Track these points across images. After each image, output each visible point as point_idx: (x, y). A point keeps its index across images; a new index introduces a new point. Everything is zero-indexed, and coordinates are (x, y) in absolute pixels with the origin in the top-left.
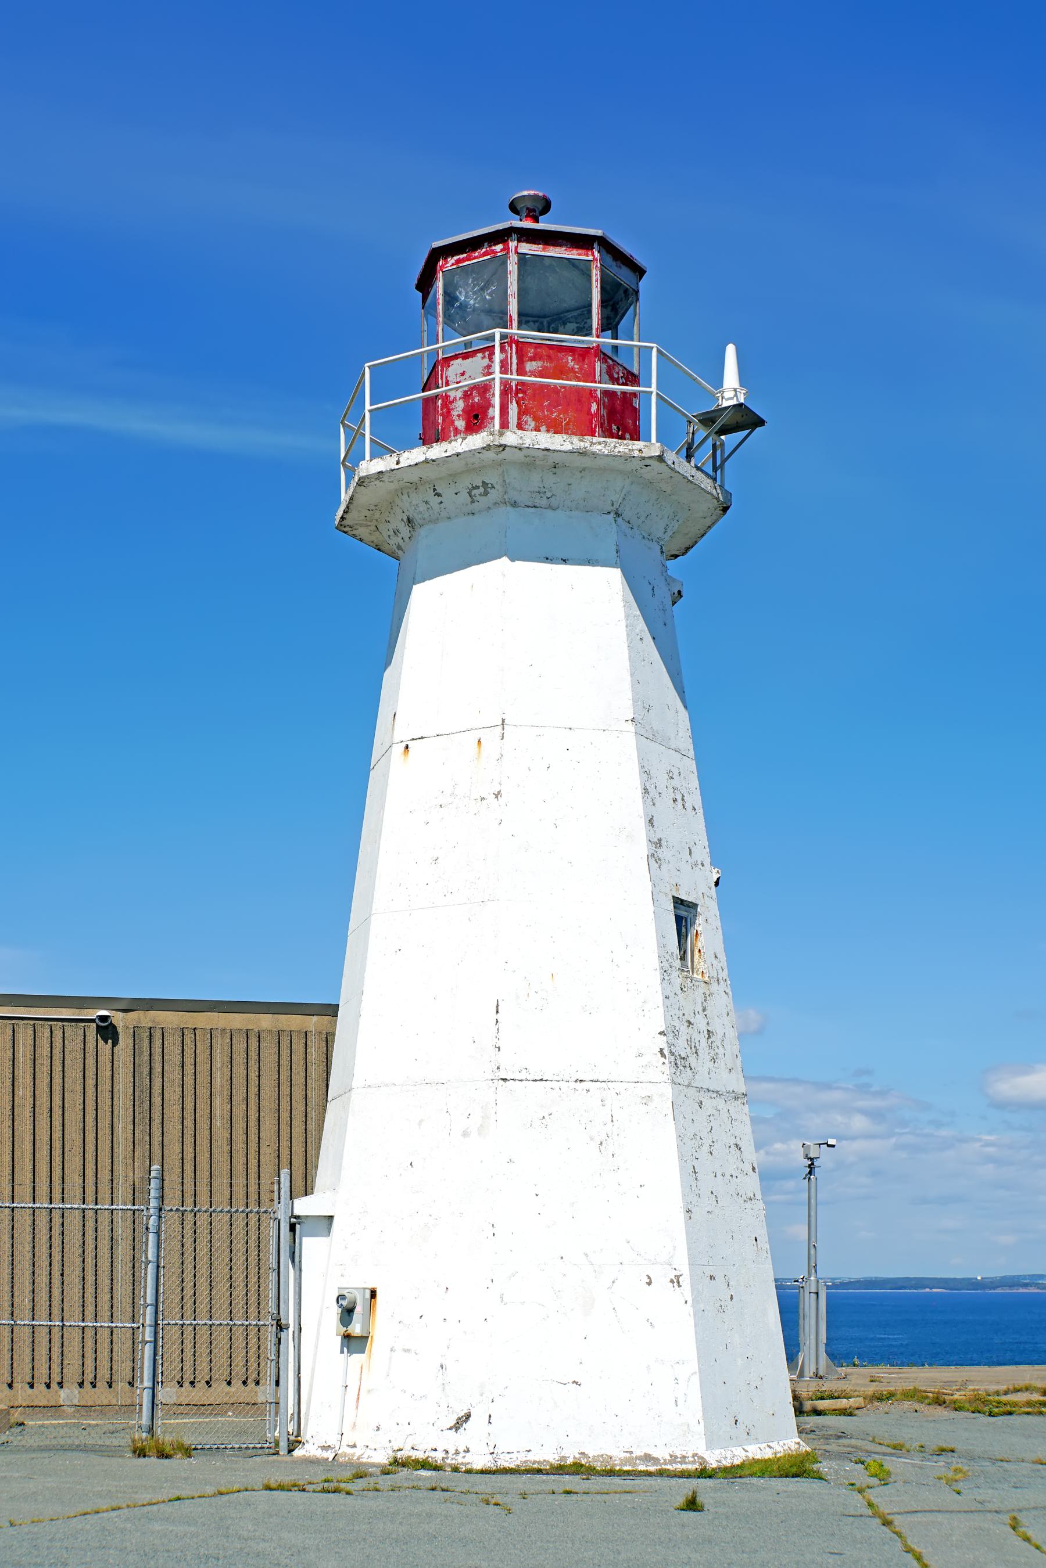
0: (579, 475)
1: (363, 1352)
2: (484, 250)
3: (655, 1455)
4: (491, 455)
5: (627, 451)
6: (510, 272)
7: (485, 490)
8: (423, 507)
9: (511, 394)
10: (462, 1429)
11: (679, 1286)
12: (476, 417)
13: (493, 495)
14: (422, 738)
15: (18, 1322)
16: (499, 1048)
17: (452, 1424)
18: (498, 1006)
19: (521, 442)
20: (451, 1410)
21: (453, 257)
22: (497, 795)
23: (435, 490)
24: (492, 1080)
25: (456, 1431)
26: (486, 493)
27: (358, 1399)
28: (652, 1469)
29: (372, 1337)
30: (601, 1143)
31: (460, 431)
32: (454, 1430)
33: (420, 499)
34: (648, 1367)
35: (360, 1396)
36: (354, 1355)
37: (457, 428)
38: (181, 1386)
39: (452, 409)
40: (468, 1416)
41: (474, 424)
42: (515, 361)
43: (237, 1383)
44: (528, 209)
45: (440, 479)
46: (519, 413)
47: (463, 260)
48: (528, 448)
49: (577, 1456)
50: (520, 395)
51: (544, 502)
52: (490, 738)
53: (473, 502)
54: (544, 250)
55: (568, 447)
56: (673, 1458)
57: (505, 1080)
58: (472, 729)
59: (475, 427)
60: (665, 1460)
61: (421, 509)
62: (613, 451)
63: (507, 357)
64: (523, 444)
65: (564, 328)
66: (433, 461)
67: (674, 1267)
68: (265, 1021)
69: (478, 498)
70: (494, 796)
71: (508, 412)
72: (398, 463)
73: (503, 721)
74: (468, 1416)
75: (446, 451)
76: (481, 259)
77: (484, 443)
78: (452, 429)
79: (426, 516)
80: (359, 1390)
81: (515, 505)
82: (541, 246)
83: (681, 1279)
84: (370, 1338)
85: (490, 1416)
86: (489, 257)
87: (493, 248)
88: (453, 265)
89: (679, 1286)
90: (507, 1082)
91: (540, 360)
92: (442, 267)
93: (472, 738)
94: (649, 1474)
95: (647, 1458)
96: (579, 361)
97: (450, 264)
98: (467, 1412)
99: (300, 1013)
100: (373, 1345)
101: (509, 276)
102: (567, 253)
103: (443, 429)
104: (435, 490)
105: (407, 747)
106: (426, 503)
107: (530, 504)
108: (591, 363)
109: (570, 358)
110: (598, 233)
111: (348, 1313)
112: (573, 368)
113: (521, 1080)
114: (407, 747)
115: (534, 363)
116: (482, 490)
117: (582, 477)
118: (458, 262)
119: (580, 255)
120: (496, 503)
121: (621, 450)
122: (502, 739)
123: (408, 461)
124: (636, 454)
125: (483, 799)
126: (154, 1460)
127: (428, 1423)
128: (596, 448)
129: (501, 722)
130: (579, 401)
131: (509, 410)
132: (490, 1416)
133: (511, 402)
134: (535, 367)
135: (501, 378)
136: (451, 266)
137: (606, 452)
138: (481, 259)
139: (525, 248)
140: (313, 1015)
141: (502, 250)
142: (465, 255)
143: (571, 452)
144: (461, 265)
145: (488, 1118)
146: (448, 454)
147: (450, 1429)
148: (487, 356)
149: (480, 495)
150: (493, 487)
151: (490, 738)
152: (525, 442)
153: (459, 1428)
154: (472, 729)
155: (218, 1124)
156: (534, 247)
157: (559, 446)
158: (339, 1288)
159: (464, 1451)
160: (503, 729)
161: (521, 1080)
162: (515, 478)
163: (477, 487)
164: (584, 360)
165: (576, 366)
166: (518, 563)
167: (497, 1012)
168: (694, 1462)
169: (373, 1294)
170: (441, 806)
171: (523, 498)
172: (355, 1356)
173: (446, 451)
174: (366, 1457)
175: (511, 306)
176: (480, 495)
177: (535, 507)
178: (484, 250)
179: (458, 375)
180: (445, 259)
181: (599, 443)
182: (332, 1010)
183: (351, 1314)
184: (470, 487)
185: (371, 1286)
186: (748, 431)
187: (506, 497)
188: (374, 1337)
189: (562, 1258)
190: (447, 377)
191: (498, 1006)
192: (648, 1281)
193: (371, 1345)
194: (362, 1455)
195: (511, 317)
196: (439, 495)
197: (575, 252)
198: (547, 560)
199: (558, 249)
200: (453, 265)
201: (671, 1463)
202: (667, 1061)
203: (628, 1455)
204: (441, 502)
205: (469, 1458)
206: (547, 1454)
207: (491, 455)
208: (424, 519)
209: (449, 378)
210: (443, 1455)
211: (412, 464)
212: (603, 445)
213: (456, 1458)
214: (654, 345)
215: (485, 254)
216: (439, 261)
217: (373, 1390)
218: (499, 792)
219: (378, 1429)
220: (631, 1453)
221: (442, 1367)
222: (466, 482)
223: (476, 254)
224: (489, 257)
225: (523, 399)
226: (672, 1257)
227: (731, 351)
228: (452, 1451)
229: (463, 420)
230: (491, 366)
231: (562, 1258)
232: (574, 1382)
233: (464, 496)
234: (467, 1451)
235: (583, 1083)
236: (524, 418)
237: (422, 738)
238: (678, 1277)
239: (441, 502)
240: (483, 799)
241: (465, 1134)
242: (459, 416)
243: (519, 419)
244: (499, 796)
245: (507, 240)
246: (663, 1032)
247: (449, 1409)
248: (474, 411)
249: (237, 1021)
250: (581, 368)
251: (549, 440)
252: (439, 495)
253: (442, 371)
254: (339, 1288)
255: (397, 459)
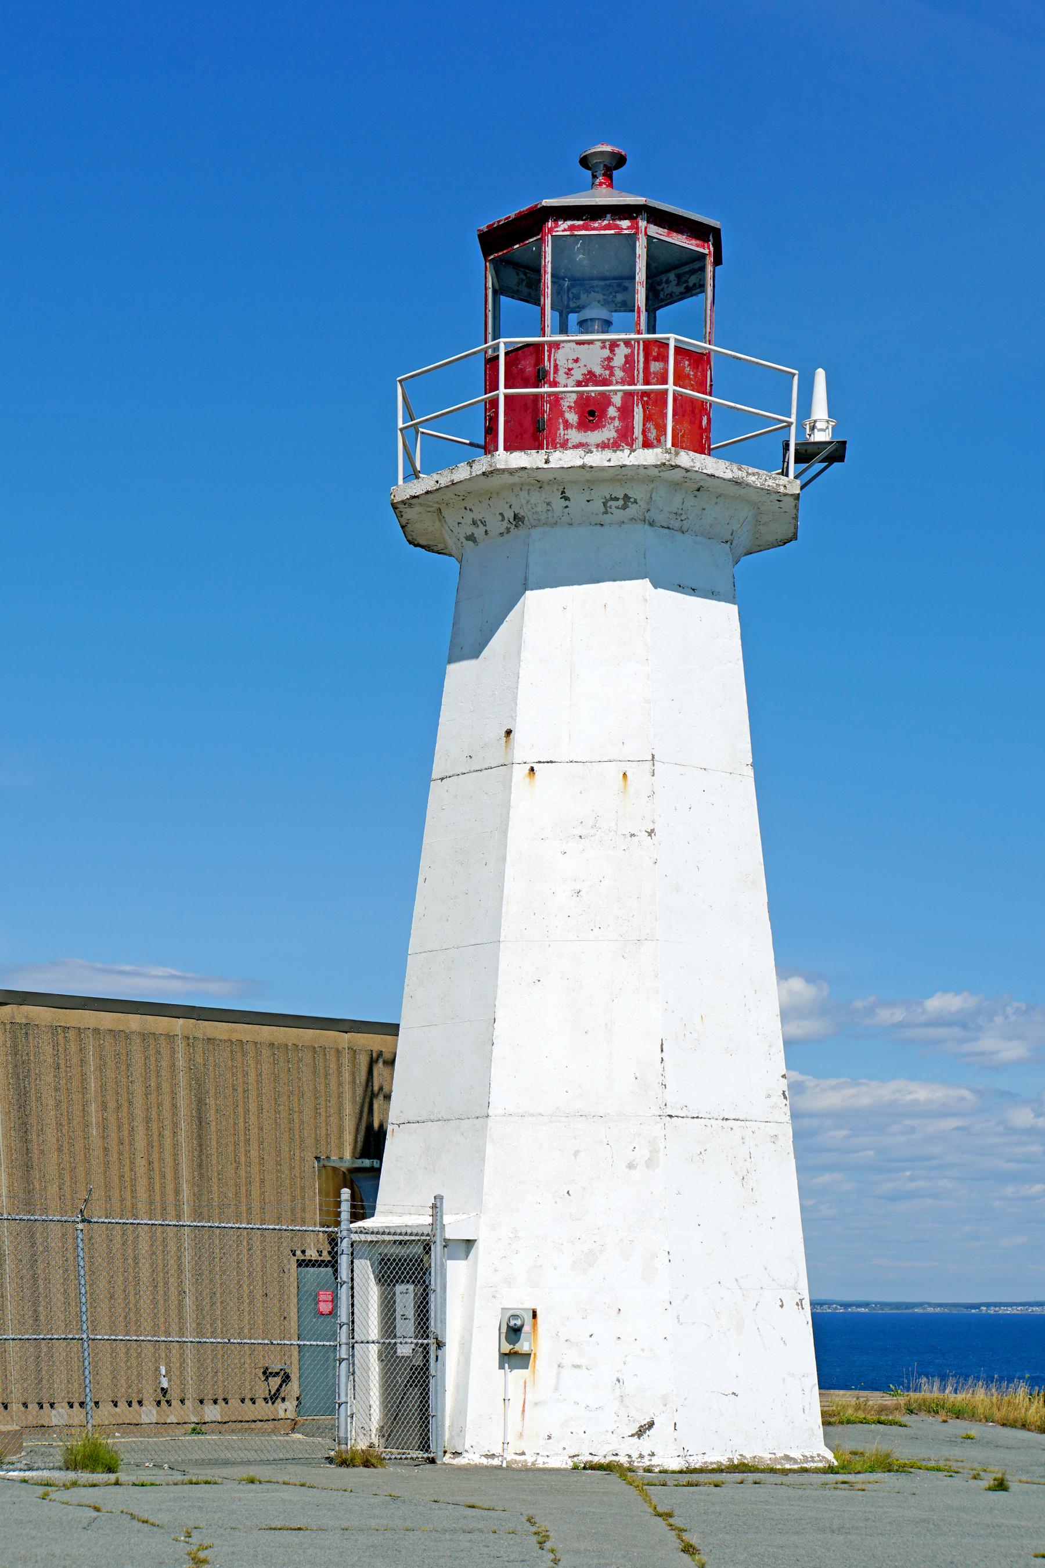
0: (714, 500)
1: (527, 1368)
2: (606, 222)
3: (792, 1455)
4: (734, 489)
5: (774, 485)
6: (639, 255)
7: (625, 503)
8: (541, 508)
9: (637, 396)
10: (645, 1436)
11: (803, 1309)
12: (592, 413)
13: (632, 510)
14: (551, 762)
15: (232, 1341)
16: (665, 1085)
17: (634, 1432)
18: (662, 1045)
19: (692, 465)
20: (632, 1419)
21: (565, 220)
22: (651, 833)
23: (563, 492)
24: (660, 1116)
25: (639, 1438)
26: (625, 507)
27: (524, 1411)
28: (796, 1467)
29: (535, 1354)
30: (743, 1178)
31: (572, 426)
32: (636, 1437)
33: (543, 499)
34: (784, 1380)
35: (526, 1408)
36: (515, 1371)
37: (567, 421)
38: (170, 1405)
39: (562, 398)
40: (651, 1425)
41: (590, 421)
42: (642, 359)
43: (122, 1405)
44: (605, 166)
45: (575, 482)
46: (644, 420)
47: (579, 228)
48: (697, 471)
49: (739, 1457)
50: (645, 399)
51: (677, 524)
52: (639, 775)
53: (606, 513)
54: (668, 236)
55: (729, 475)
56: (806, 1459)
57: (670, 1116)
58: (614, 761)
59: (591, 425)
60: (801, 1460)
61: (539, 509)
62: (764, 484)
63: (633, 353)
64: (694, 467)
65: (588, 296)
66: (591, 467)
67: (799, 1291)
68: (134, 1022)
69: (614, 510)
70: (647, 834)
71: (633, 416)
72: (547, 462)
73: (653, 756)
74: (651, 1425)
75: (609, 460)
76: (602, 232)
77: (657, 460)
78: (561, 421)
79: (543, 518)
80: (524, 1403)
81: (652, 524)
82: (666, 230)
83: (803, 1301)
84: (532, 1356)
85: (675, 1424)
86: (612, 232)
87: (618, 222)
88: (565, 230)
89: (803, 1309)
90: (673, 1119)
91: (662, 361)
92: (551, 230)
93: (614, 772)
94: (791, 1471)
95: (787, 1458)
96: (694, 368)
97: (561, 228)
98: (649, 1420)
99: (174, 1015)
100: (537, 1362)
101: (637, 260)
102: (687, 242)
103: (549, 419)
104: (563, 492)
105: (532, 769)
106: (548, 504)
107: (665, 525)
108: (704, 371)
109: (687, 363)
110: (640, 200)
111: (514, 1332)
112: (689, 375)
113: (683, 1117)
114: (532, 769)
115: (657, 363)
116: (621, 503)
117: (716, 503)
118: (572, 228)
119: (698, 246)
120: (632, 519)
121: (771, 484)
122: (653, 776)
123: (561, 462)
124: (782, 490)
125: (633, 835)
126: (362, 1469)
127: (607, 1431)
128: (751, 479)
129: (650, 758)
130: (693, 412)
131: (635, 413)
132: (675, 1424)
133: (637, 405)
134: (658, 369)
135: (674, 390)
136: (563, 231)
137: (759, 485)
138: (602, 232)
139: (654, 231)
140: (179, 1018)
141: (628, 228)
142: (581, 223)
143: (730, 480)
144: (576, 233)
145: (657, 1152)
146: (611, 464)
147: (633, 1435)
148: (608, 346)
149: (617, 508)
150: (635, 502)
151: (639, 775)
152: (695, 465)
153: (642, 1435)
154: (614, 761)
155: (94, 1133)
156: (660, 230)
157: (722, 473)
158: (502, 1309)
159: (649, 1455)
160: (654, 765)
161: (683, 1117)
162: (661, 497)
163: (617, 499)
164: (698, 368)
165: (692, 373)
166: (660, 590)
167: (662, 1051)
168: (821, 1461)
169: (535, 1315)
170: (580, 837)
171: (661, 518)
172: (517, 1372)
173: (609, 460)
174: (542, 1463)
175: (639, 294)
176: (617, 508)
177: (668, 528)
178: (606, 222)
179: (570, 361)
180: (556, 221)
181: (754, 474)
182: (393, 1029)
183: (518, 1333)
184: (608, 497)
185: (533, 1307)
186: (826, 464)
187: (647, 515)
188: (537, 1354)
189: (719, 1283)
190: (555, 360)
191: (662, 1045)
192: (781, 1304)
193: (535, 1361)
194: (536, 1461)
195: (639, 308)
196: (567, 499)
197: (694, 242)
198: (680, 588)
199: (680, 236)
200: (565, 230)
201: (807, 1462)
202: (788, 1103)
203: (773, 1456)
204: (567, 507)
205: (655, 1461)
206: (718, 1456)
207: (734, 489)
208: (539, 520)
209: (558, 362)
210: (626, 1459)
211: (565, 466)
212: (756, 477)
213: (642, 1461)
214: (796, 372)
215: (606, 228)
216: (548, 222)
217: (540, 1402)
218: (653, 831)
219: (549, 1437)
220: (774, 1454)
221: (619, 1381)
222: (606, 491)
223: (596, 225)
224: (612, 232)
225: (647, 403)
226: (796, 1283)
227: (820, 375)
228: (635, 1455)
229: (576, 413)
230: (612, 359)
231: (719, 1283)
232: (734, 1393)
233: (597, 505)
234: (653, 1454)
235: (728, 1121)
236: (648, 425)
237: (551, 762)
238: (801, 1300)
239: (567, 507)
240: (633, 835)
241: (631, 1166)
242: (570, 407)
243: (644, 425)
244: (653, 835)
245: (636, 217)
246: (785, 1075)
247: (629, 1418)
248: (589, 406)
249: (107, 1020)
250: (695, 375)
251: (714, 465)
252: (567, 499)
253: (550, 351)
254: (502, 1309)
255: (546, 457)
